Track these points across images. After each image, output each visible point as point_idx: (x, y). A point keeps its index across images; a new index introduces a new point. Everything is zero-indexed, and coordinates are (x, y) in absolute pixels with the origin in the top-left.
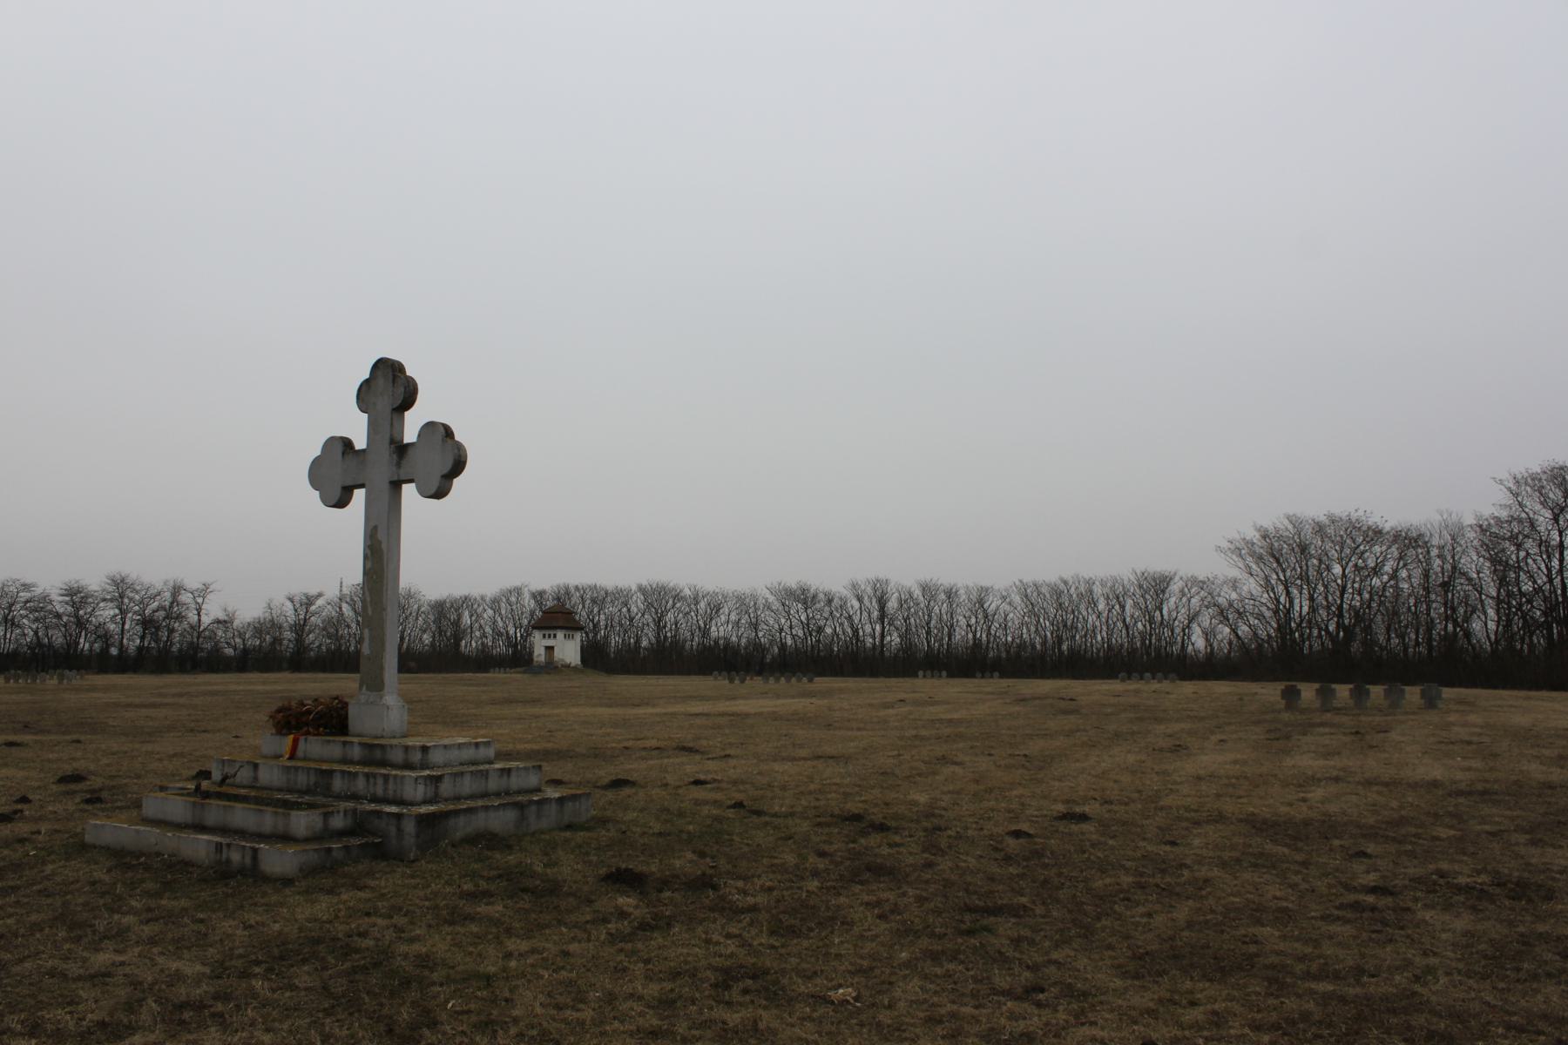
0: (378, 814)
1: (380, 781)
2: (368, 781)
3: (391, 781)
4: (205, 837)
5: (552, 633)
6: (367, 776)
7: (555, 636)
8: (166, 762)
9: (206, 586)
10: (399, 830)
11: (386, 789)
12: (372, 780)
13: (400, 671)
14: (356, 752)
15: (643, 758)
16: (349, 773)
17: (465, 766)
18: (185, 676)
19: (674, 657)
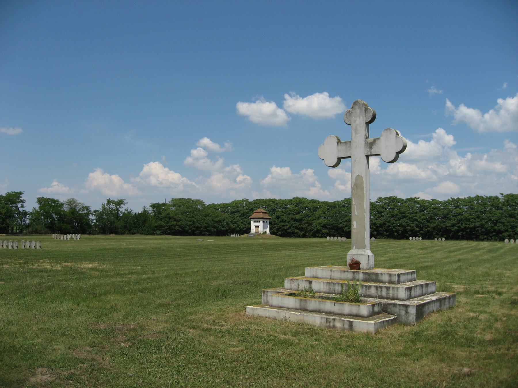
0: (395, 305)
1: (384, 290)
2: (377, 289)
3: (391, 289)
4: (274, 309)
5: (258, 220)
6: (376, 287)
7: (259, 222)
8: (439, 342)
9: (366, 155)
10: (407, 312)
11: (388, 294)
12: (379, 289)
13: (371, 236)
14: (361, 276)
15: (288, 251)
16: (366, 286)
17: (177, 240)
18: (315, 239)
19: (474, 233)
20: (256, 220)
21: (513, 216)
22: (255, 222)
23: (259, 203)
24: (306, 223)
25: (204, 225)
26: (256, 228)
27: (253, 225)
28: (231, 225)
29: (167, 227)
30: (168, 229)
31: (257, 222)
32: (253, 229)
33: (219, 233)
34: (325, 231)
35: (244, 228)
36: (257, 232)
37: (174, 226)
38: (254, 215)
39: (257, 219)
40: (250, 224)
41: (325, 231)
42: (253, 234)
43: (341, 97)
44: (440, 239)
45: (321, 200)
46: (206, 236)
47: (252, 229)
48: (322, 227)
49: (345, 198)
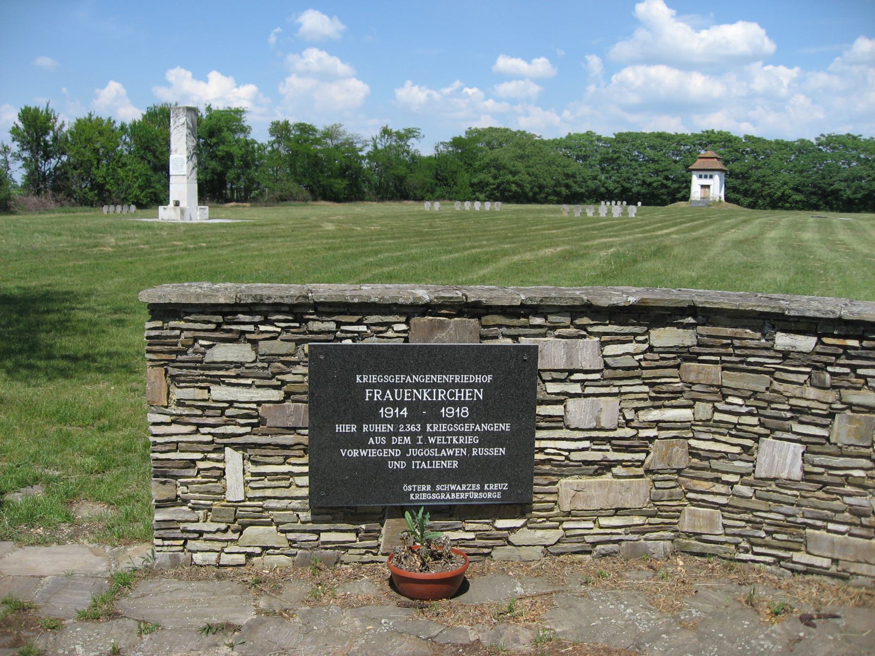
5: (708, 173)
20: (703, 173)
21: (340, 184)
22: (700, 177)
23: (709, 140)
24: (758, 181)
25: (550, 182)
26: (703, 190)
27: (696, 183)
28: (589, 183)
29: (494, 186)
30: (495, 189)
31: (706, 177)
32: (696, 192)
33: (574, 198)
34: (798, 197)
35: (615, 189)
36: (703, 198)
37: (508, 182)
38: (699, 164)
39: (707, 172)
40: (688, 182)
41: (798, 197)
42: (696, 202)
43: (546, 57)
44: (619, 203)
45: (811, 137)
46: (553, 204)
47: (695, 192)
48: (793, 189)
49: (775, 138)
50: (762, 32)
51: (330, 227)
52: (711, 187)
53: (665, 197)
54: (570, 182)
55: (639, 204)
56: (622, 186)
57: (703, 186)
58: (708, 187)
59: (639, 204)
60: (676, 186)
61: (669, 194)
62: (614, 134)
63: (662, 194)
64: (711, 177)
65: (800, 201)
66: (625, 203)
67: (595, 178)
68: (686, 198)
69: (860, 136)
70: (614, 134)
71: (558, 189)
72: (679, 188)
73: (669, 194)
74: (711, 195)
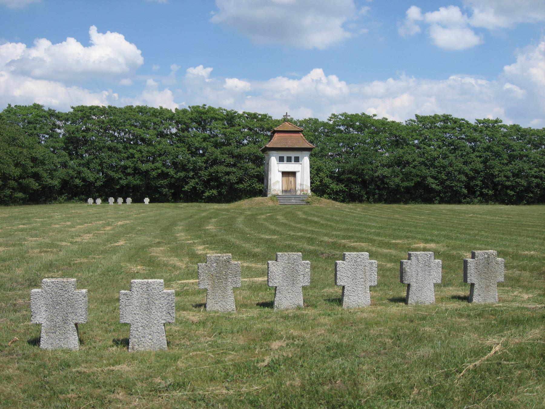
5: (293, 155)
20: (285, 154)
22: (281, 160)
26: (285, 178)
31: (289, 160)
36: (286, 191)
50: (139, 52)
51: (249, 97)
52: (298, 175)
53: (165, 190)
54: (39, 169)
55: (147, 200)
56: (107, 175)
57: (285, 174)
58: (293, 174)
59: (147, 200)
60: (182, 174)
61: (170, 186)
62: (72, 108)
63: (162, 186)
64: (297, 160)
65: (341, 191)
66: (129, 200)
67: (65, 165)
68: (263, 193)
69: (375, 115)
70: (72, 108)
71: (24, 182)
72: (186, 177)
73: (170, 186)
74: (298, 187)
